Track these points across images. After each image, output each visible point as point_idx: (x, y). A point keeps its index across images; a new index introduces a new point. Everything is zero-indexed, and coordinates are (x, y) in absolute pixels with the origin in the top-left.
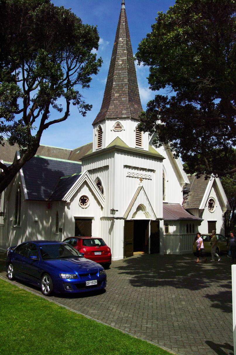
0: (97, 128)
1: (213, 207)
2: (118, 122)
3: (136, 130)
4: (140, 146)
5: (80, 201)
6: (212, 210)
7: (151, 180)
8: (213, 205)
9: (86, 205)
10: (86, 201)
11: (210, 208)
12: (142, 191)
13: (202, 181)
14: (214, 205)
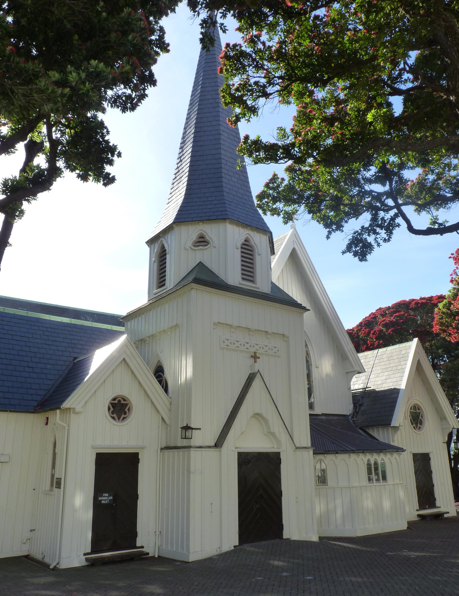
0: (157, 247)
1: (421, 423)
2: (201, 230)
3: (242, 248)
4: (252, 281)
5: (109, 409)
6: (420, 428)
7: (279, 357)
8: (420, 418)
9: (124, 418)
10: (126, 410)
11: (414, 425)
12: (257, 383)
13: (392, 365)
14: (422, 417)
